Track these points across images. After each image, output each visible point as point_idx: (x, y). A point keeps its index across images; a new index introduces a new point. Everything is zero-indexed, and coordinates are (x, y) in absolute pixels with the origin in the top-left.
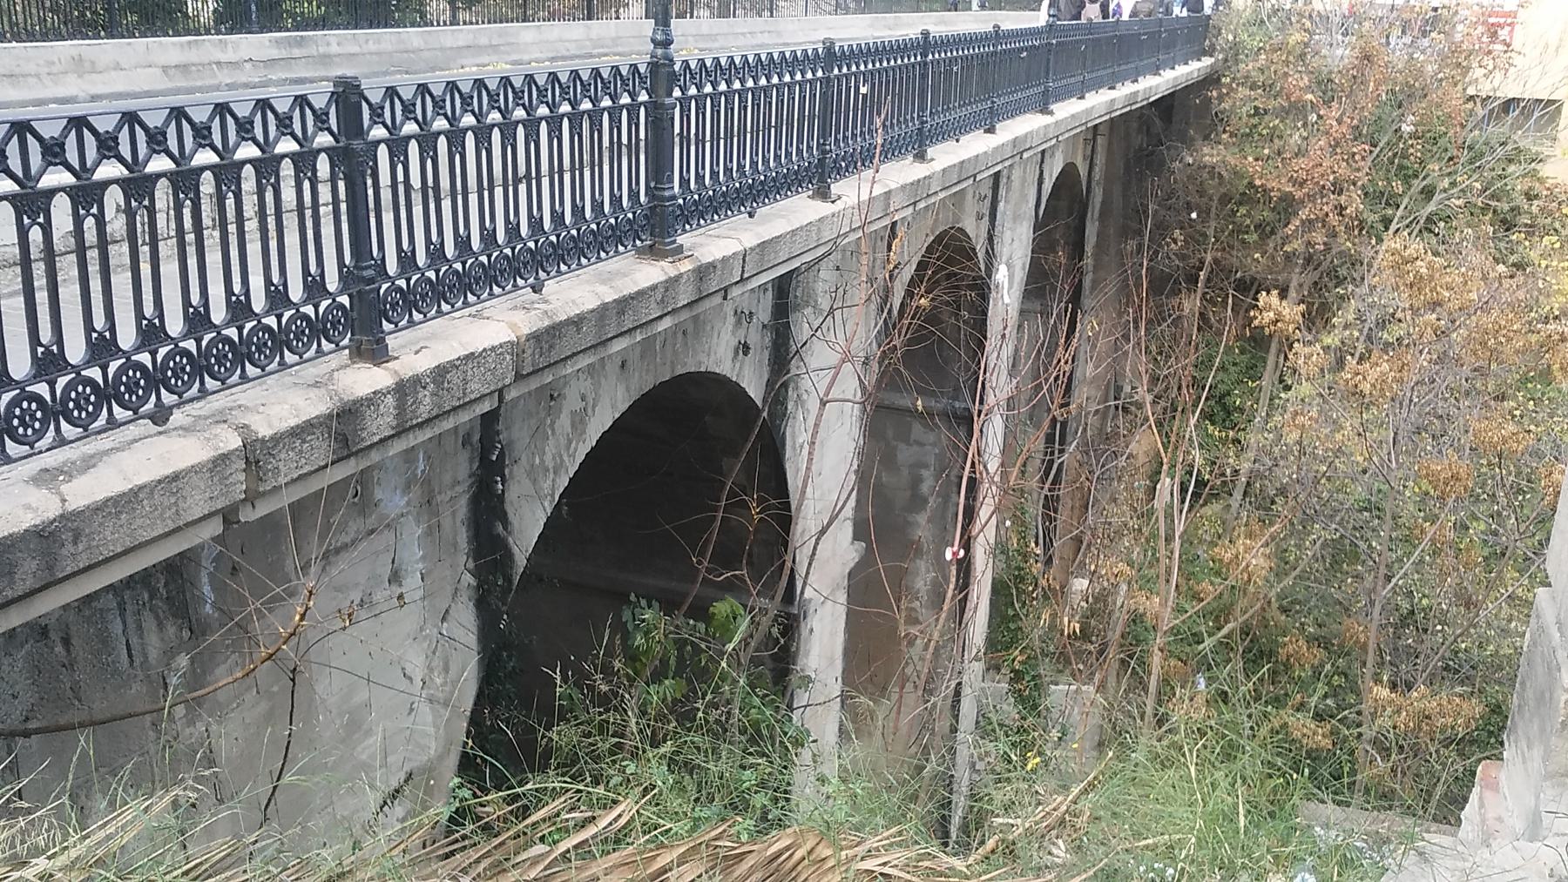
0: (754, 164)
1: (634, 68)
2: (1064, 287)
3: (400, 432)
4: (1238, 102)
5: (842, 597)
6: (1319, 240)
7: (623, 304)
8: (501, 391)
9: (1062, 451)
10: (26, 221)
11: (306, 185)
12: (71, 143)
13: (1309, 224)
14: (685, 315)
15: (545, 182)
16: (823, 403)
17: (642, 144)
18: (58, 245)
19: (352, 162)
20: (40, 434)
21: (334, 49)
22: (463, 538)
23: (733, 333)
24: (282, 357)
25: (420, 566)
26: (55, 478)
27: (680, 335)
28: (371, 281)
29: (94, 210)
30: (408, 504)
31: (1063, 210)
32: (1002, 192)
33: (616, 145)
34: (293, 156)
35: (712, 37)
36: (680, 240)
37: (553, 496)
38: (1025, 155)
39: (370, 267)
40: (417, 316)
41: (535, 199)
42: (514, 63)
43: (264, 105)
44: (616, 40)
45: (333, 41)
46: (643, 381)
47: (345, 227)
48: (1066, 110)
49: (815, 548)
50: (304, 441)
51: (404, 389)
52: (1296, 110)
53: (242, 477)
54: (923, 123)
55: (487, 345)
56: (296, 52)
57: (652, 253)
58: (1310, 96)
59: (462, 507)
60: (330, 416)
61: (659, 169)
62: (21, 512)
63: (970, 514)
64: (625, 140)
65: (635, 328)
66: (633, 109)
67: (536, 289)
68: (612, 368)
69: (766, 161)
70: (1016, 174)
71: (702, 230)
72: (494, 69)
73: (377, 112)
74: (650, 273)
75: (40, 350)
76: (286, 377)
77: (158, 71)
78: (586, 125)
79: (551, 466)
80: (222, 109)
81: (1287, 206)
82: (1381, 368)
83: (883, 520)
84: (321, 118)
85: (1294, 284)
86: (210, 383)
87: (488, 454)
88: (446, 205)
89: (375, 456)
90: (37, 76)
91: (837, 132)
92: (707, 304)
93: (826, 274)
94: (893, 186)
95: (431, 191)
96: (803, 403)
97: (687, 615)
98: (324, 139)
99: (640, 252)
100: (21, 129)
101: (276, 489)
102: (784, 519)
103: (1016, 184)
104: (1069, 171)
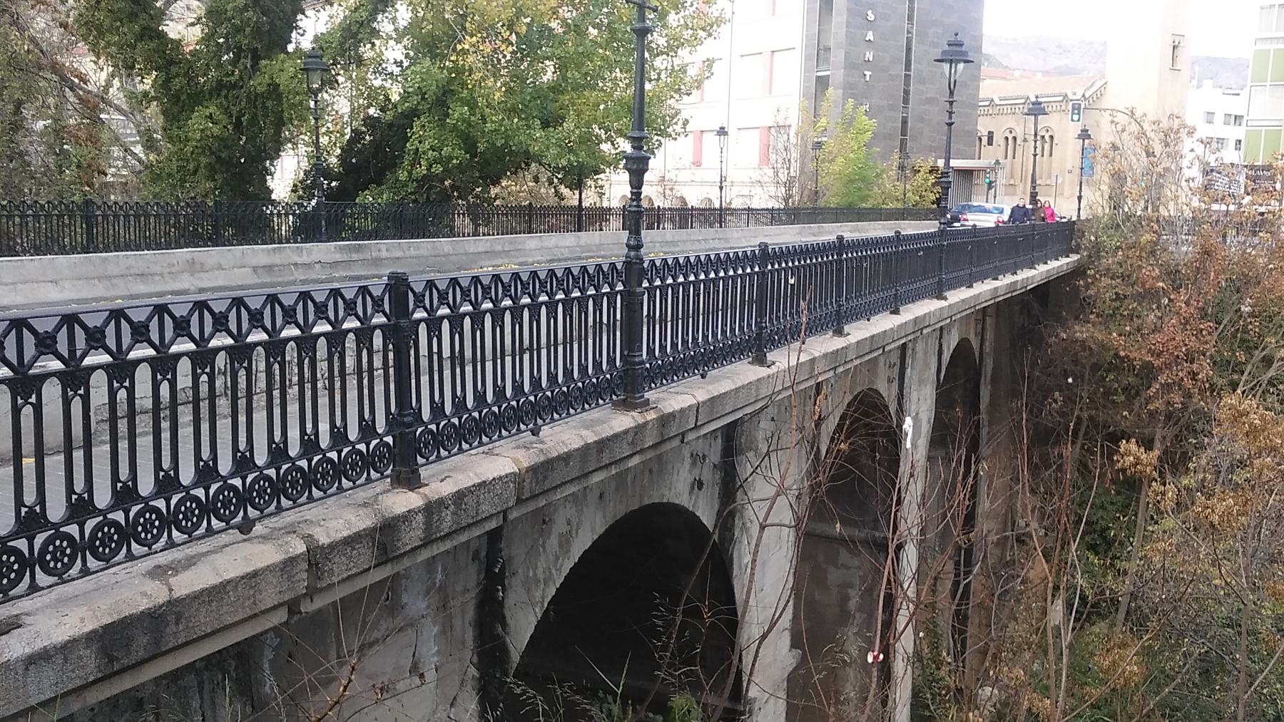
0: (705, 337)
1: (613, 266)
2: (963, 437)
3: (427, 543)
4: (1104, 289)
5: (783, 695)
6: (1177, 400)
7: (602, 445)
8: (505, 512)
9: (968, 573)
10: (116, 385)
11: (365, 353)
12: (110, 331)
13: (1167, 387)
14: (650, 454)
15: (544, 352)
16: (762, 528)
17: (618, 323)
18: (181, 397)
19: (400, 336)
20: (156, 539)
21: (384, 254)
22: (470, 635)
23: (690, 472)
24: (340, 483)
25: (436, 659)
26: (166, 572)
27: (647, 473)
28: (410, 425)
29: (33, 399)
30: (428, 607)
31: (959, 379)
32: (909, 360)
33: (598, 324)
34: (355, 331)
35: (674, 243)
36: (647, 395)
37: (542, 603)
38: (925, 331)
39: (409, 415)
40: (443, 453)
41: (535, 364)
42: (520, 264)
43: (273, 299)
44: (600, 246)
45: (383, 248)
46: (616, 510)
47: (392, 386)
48: (957, 296)
49: (757, 651)
50: (353, 549)
51: (432, 508)
52: (1150, 295)
53: (305, 576)
54: (840, 306)
55: (495, 475)
56: (355, 256)
57: (626, 405)
58: (1161, 284)
59: (471, 613)
60: (374, 529)
61: (631, 341)
62: (139, 598)
63: (889, 624)
64: (605, 321)
65: (611, 464)
66: (611, 297)
67: (535, 432)
68: (592, 498)
69: (715, 335)
70: (920, 347)
71: (664, 388)
72: (507, 268)
73: (419, 299)
74: (623, 421)
75: (162, 474)
76: (343, 499)
77: (249, 270)
78: (575, 310)
79: (542, 577)
80: (305, 296)
81: (1148, 373)
82: (1224, 504)
83: (814, 630)
84: (378, 303)
85: (1158, 437)
86: (285, 502)
87: (492, 562)
88: (469, 369)
89: (406, 562)
90: (161, 275)
91: (771, 313)
92: (668, 446)
93: (765, 425)
94: (817, 354)
95: (457, 359)
96: (747, 530)
97: (649, 709)
98: (379, 319)
99: (616, 405)
100: (19, 325)
101: (331, 586)
102: (733, 624)
103: (920, 355)
104: (963, 345)
